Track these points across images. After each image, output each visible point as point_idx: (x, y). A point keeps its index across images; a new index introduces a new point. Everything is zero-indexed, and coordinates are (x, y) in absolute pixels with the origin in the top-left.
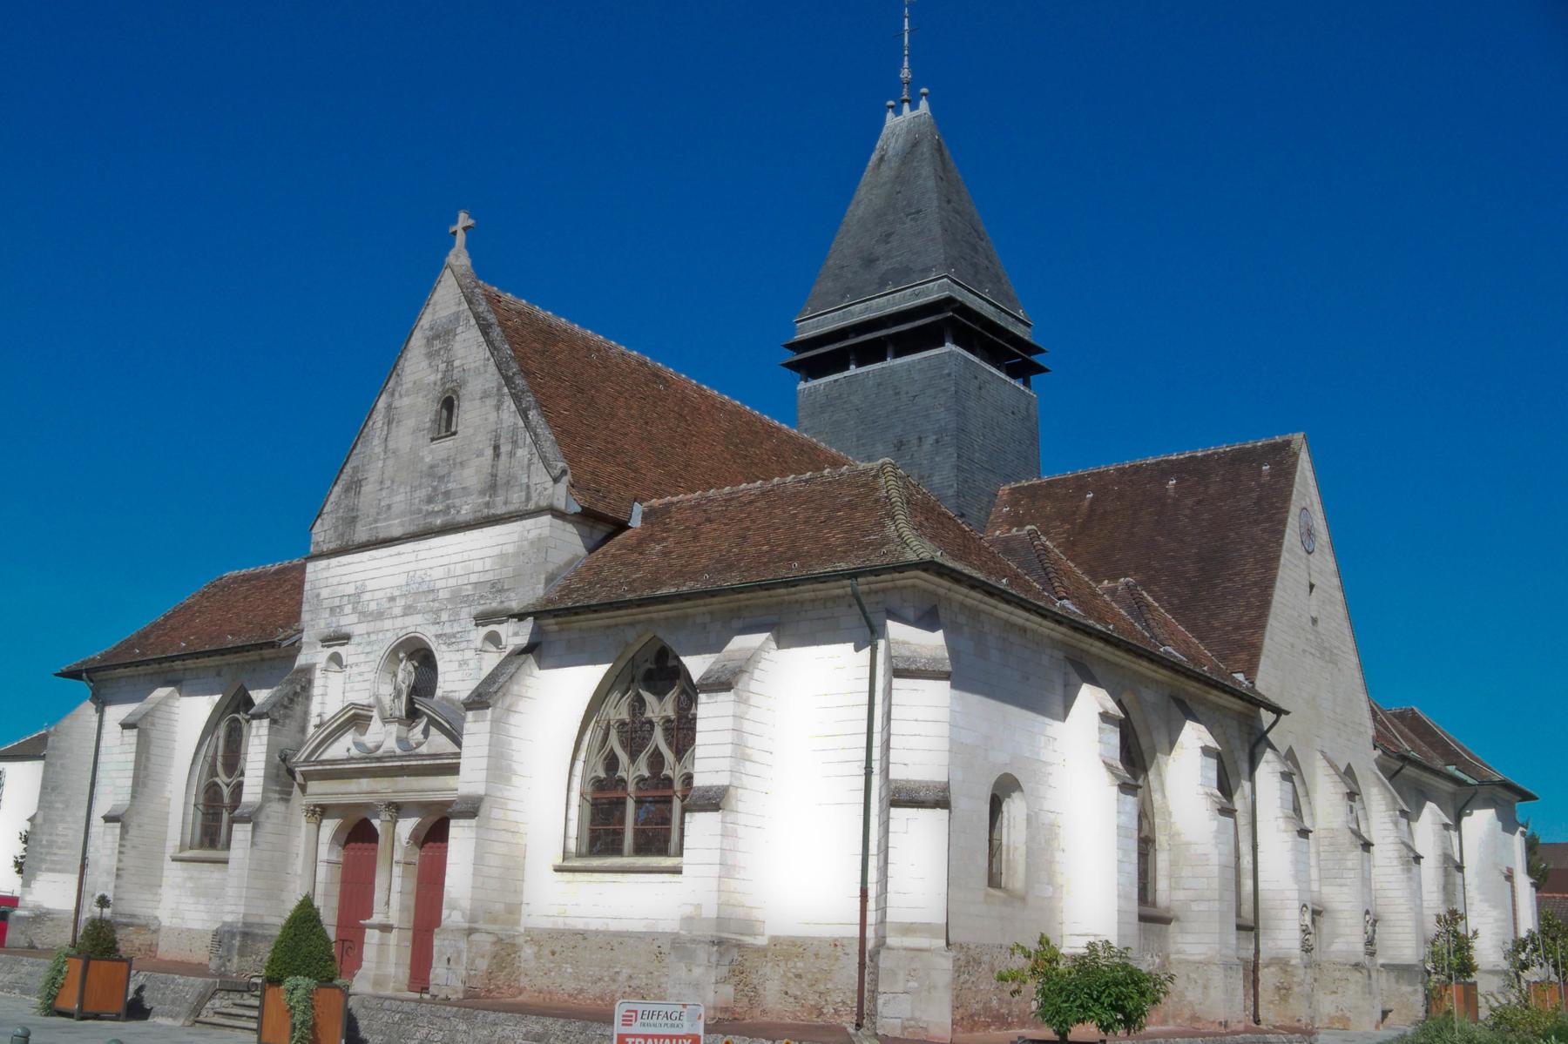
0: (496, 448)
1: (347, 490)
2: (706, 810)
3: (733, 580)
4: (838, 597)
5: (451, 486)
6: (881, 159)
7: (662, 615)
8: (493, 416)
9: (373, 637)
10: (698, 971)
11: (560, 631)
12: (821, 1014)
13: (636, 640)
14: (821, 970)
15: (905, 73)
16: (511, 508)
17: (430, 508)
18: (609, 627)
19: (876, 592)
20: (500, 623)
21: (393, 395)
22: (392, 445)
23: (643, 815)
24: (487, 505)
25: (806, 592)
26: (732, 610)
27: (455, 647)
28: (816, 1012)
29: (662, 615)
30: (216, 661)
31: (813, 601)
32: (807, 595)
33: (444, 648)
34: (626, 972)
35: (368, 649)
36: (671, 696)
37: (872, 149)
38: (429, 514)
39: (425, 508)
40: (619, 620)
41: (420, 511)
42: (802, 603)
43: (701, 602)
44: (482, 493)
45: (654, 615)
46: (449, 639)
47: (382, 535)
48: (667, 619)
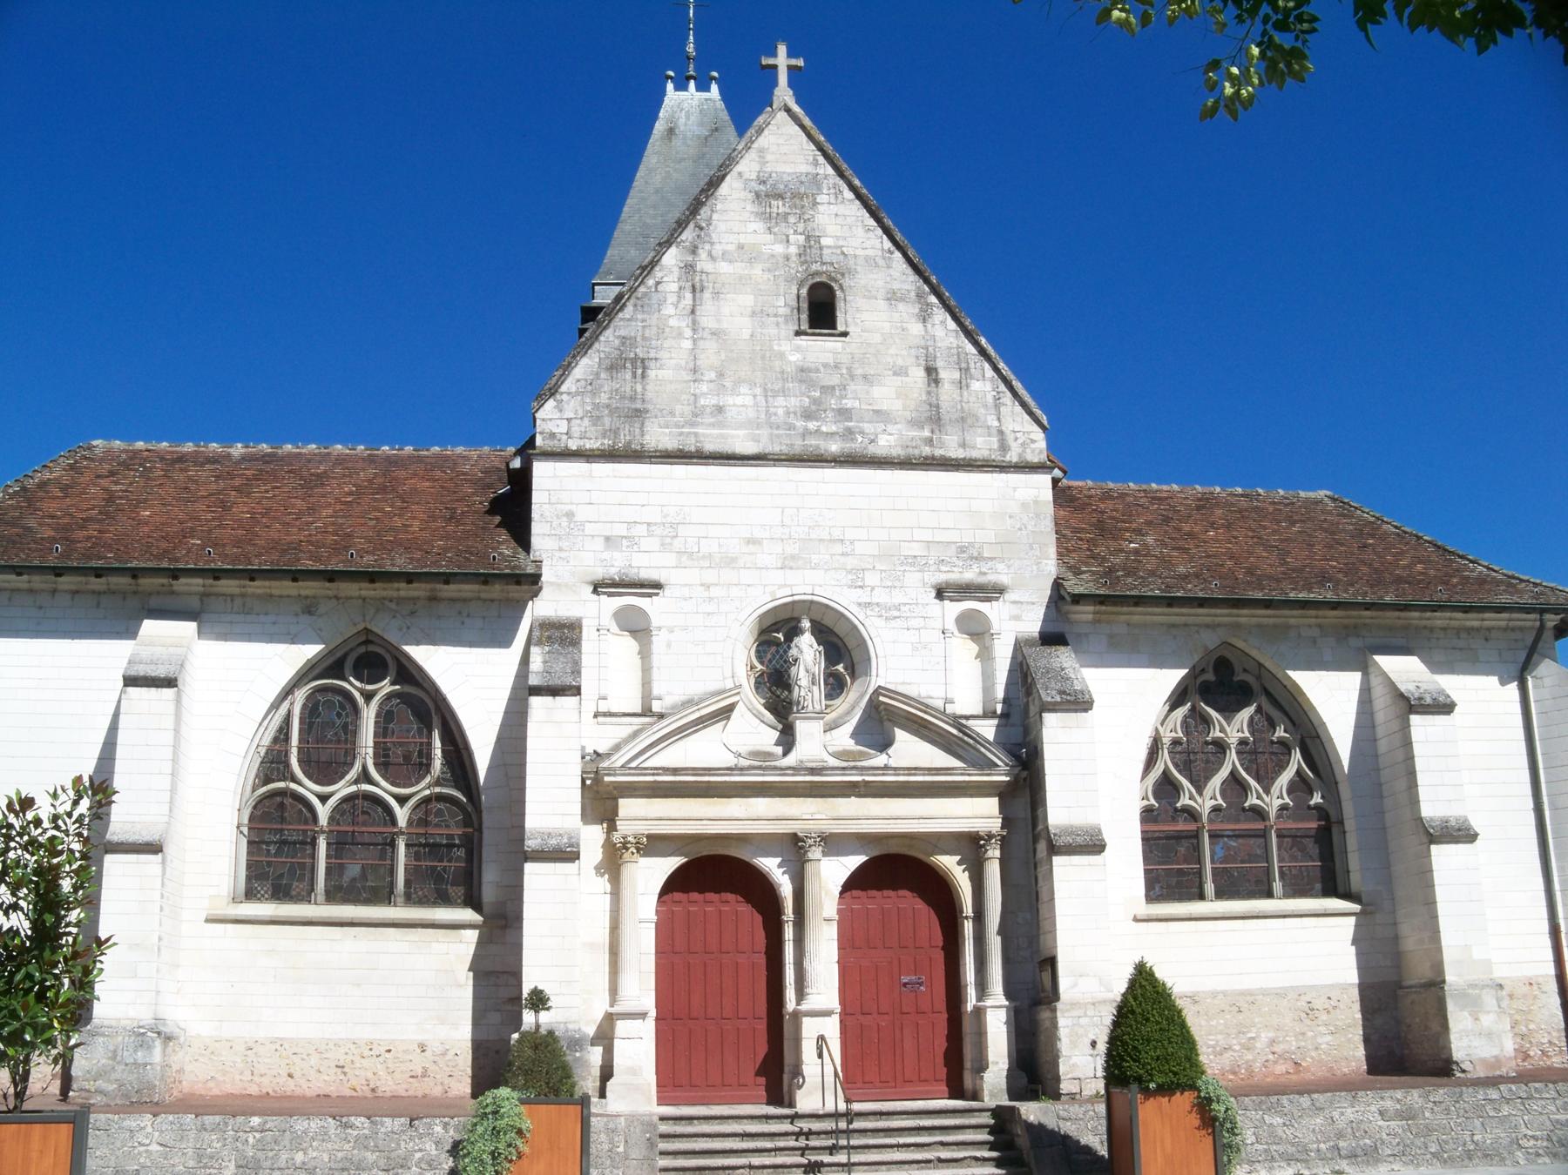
0: (931, 371)
1: (614, 366)
2: (1457, 842)
3: (400, 563)
4: (1472, 629)
5: (848, 403)
6: (671, 131)
7: (1254, 620)
8: (916, 328)
9: (714, 592)
10: (1487, 1020)
11: (1096, 622)
12: (1526, 1057)
13: (345, 627)
14: (1519, 1011)
15: (691, 48)
16: (975, 454)
17: (812, 425)
18: (1173, 626)
19: (1513, 629)
20: (989, 600)
21: (694, 250)
22: (706, 320)
23: (1220, 853)
24: (930, 442)
25: (1440, 619)
26: (1346, 627)
27: (898, 623)
28: (1521, 1056)
29: (1254, 620)
30: (1159, 615)
31: (1444, 629)
32: (1439, 623)
33: (881, 623)
34: (1265, 1036)
35: (711, 608)
36: (1246, 714)
37: (655, 117)
38: (806, 433)
39: (800, 424)
40: (1191, 620)
41: (791, 427)
42: (1432, 629)
43: (1313, 613)
44: (915, 423)
45: (1243, 620)
46: (891, 613)
47: (709, 447)
48: (1259, 626)
